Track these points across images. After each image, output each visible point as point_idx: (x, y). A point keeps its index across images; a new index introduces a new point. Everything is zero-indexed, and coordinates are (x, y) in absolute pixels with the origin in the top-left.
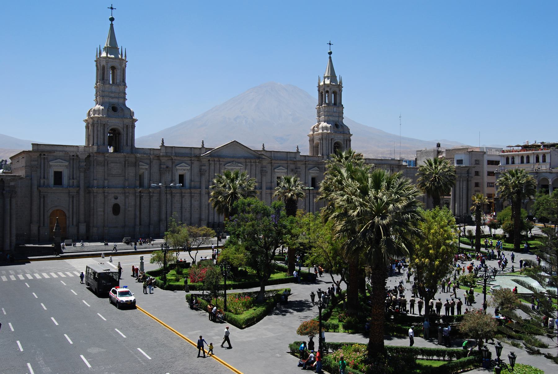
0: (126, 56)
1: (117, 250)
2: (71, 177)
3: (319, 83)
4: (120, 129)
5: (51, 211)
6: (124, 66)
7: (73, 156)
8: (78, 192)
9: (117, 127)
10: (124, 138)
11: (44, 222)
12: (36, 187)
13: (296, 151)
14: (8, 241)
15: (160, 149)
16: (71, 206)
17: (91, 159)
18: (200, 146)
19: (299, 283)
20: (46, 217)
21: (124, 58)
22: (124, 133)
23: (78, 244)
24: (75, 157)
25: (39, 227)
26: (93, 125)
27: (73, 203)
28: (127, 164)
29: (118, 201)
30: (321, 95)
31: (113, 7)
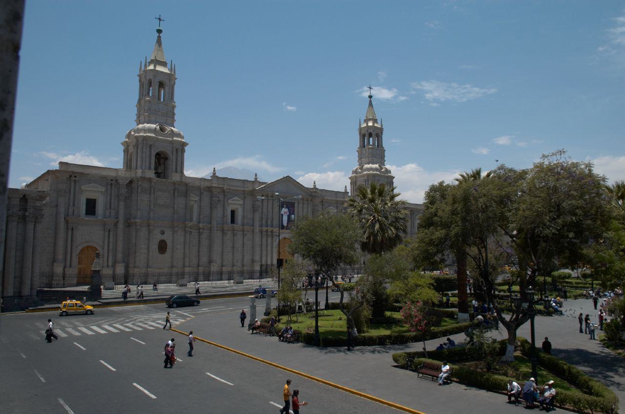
0: (175, 71)
1: (143, 297)
2: (108, 207)
3: (360, 125)
4: (168, 152)
5: (80, 248)
6: (172, 82)
7: (112, 180)
8: (116, 225)
9: (163, 150)
10: (171, 163)
11: (71, 262)
12: (63, 216)
13: (344, 191)
14: (28, 282)
15: (211, 180)
16: (106, 241)
17: (134, 185)
18: (253, 180)
19: (436, 338)
20: (74, 254)
21: (173, 73)
22: (172, 157)
23: (435, 272)
24: (113, 182)
25: (65, 267)
26: (134, 147)
27: (109, 239)
28: (176, 194)
29: (164, 237)
30: (363, 137)
31: (158, 17)
